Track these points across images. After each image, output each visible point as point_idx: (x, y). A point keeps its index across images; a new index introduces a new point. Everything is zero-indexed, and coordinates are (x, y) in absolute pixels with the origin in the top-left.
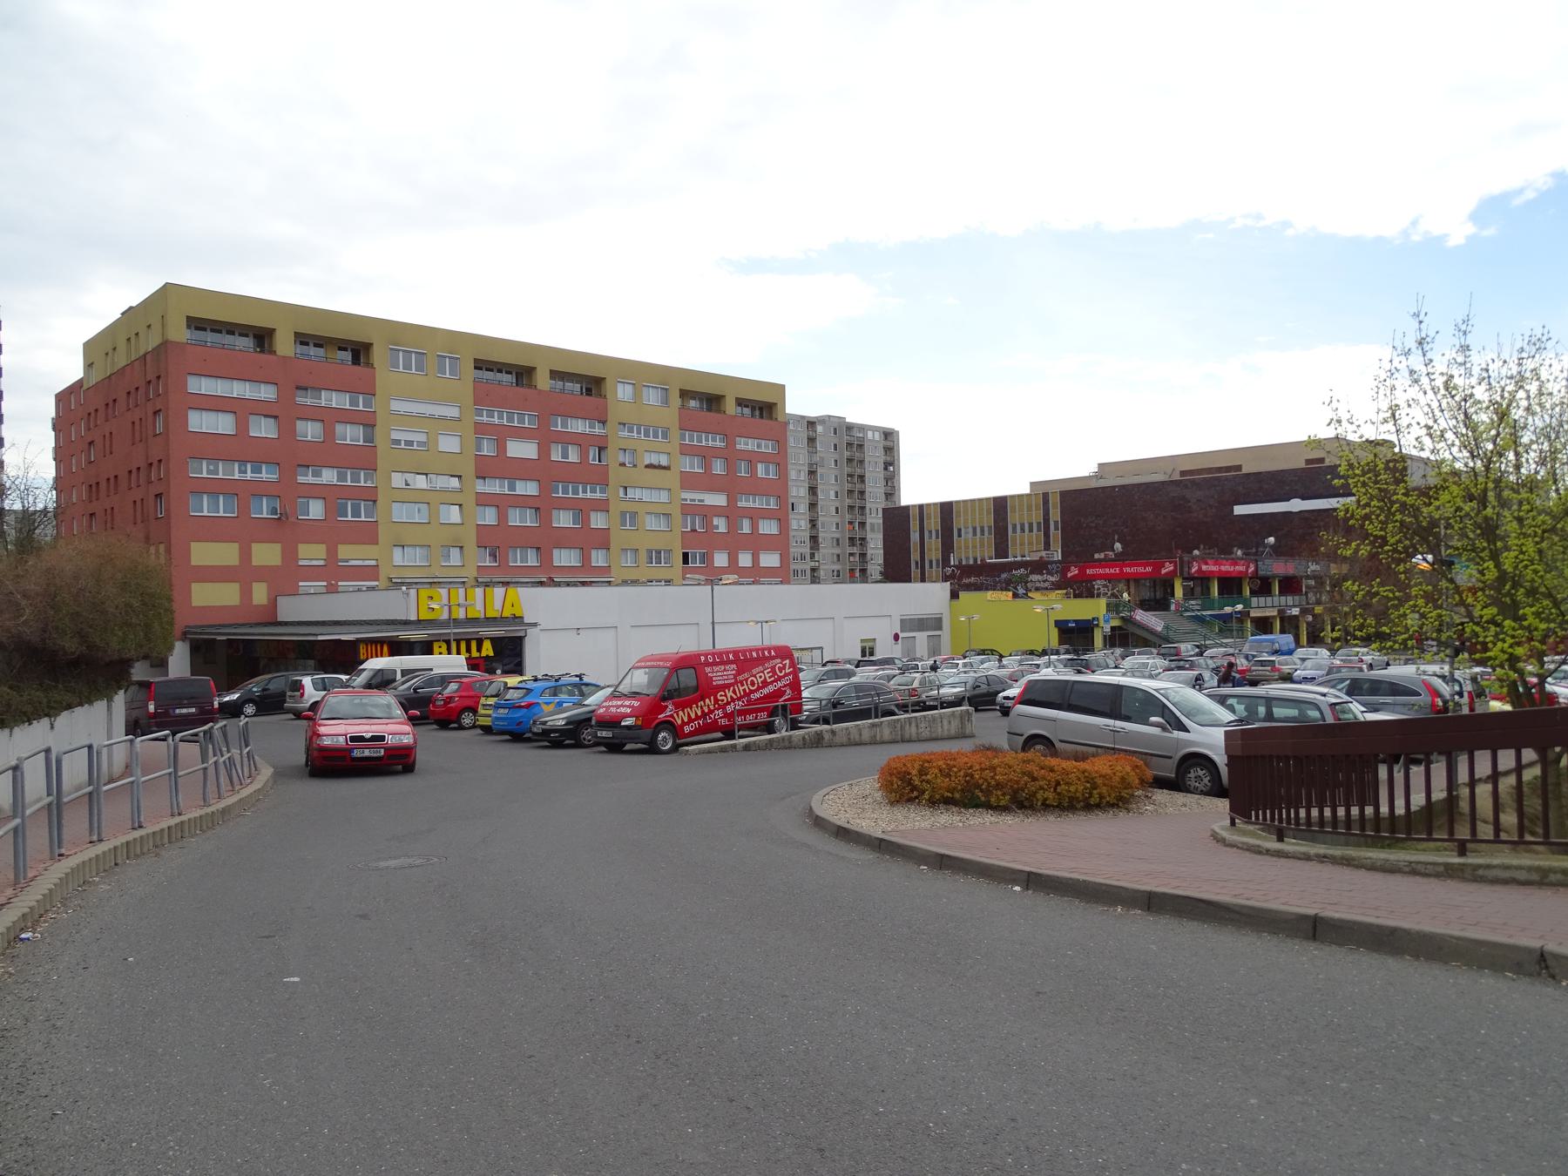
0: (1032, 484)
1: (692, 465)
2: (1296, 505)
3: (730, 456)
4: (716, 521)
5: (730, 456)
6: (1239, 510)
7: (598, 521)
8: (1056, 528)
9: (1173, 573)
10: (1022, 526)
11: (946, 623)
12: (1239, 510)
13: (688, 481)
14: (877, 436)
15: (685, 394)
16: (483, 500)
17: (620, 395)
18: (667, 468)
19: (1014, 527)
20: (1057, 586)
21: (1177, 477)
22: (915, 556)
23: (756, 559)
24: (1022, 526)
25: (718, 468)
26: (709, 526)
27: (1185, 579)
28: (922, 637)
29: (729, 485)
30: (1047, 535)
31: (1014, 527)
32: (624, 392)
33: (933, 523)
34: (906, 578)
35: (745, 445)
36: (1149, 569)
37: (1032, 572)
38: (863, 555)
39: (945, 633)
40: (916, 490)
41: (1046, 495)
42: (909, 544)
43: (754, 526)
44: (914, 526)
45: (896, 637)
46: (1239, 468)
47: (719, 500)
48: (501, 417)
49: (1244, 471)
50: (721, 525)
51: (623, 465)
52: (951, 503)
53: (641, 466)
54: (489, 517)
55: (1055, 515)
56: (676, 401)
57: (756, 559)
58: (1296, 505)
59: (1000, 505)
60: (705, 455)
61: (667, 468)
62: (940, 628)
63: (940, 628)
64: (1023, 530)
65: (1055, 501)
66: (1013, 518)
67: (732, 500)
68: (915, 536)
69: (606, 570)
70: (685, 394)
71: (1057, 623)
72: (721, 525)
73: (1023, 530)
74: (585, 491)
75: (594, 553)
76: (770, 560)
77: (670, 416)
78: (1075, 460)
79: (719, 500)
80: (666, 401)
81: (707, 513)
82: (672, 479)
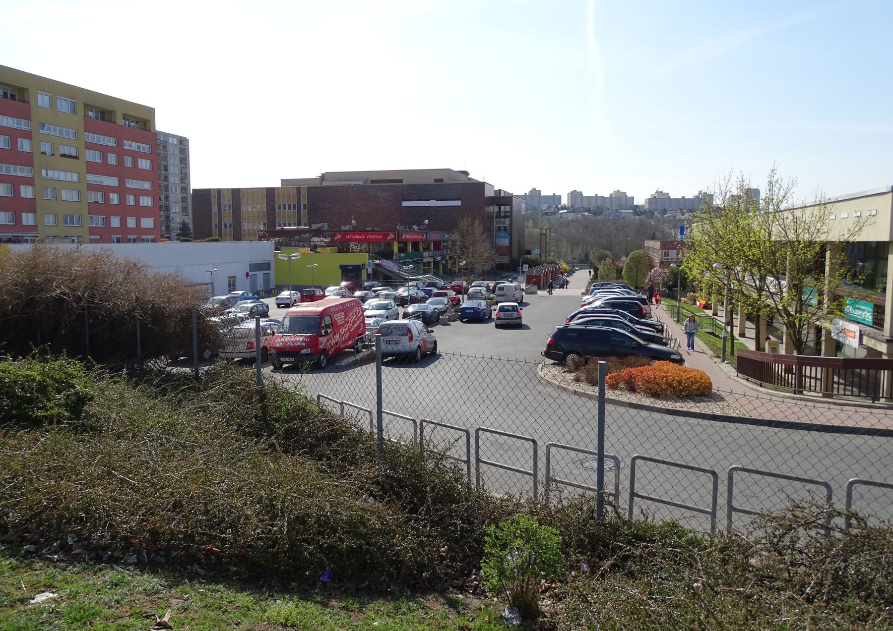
0: (282, 180)
1: (94, 156)
2: (433, 203)
3: (121, 153)
4: (111, 195)
5: (121, 153)
6: (405, 204)
7: (26, 192)
8: (305, 208)
9: (394, 239)
10: (284, 206)
11: (273, 266)
12: (405, 204)
13: (92, 168)
14: (175, 141)
15: (87, 106)
16: (92, 187)
17: (40, 103)
18: (76, 158)
19: (279, 206)
20: (328, 245)
21: (369, 184)
22: (215, 221)
23: (138, 222)
24: (284, 206)
25: (112, 159)
26: (106, 198)
27: (399, 243)
28: (260, 274)
29: (119, 172)
30: (299, 212)
31: (279, 206)
32: (43, 100)
33: (227, 201)
34: (240, 239)
35: (131, 146)
36: (381, 237)
37: (314, 236)
38: (167, 217)
39: (272, 272)
40: (201, 178)
41: (298, 189)
42: (213, 216)
43: (137, 201)
44: (214, 202)
45: (247, 275)
46: (401, 181)
47: (113, 182)
48: (55, 131)
49: (404, 183)
50: (114, 198)
51: (44, 153)
52: (239, 189)
53: (57, 155)
54: (98, 197)
55: (304, 201)
56: (80, 110)
57: (138, 222)
58: (433, 203)
59: (270, 193)
60: (104, 150)
61: (76, 158)
62: (269, 269)
63: (269, 269)
64: (284, 208)
65: (304, 193)
66: (279, 201)
67: (122, 182)
68: (215, 209)
69: (33, 228)
70: (87, 106)
71: (341, 267)
72: (114, 198)
73: (284, 208)
74: (15, 171)
75: (24, 215)
76: (147, 223)
77: (78, 120)
78: (309, 170)
79: (113, 182)
80: (74, 111)
81: (106, 190)
82: (80, 165)
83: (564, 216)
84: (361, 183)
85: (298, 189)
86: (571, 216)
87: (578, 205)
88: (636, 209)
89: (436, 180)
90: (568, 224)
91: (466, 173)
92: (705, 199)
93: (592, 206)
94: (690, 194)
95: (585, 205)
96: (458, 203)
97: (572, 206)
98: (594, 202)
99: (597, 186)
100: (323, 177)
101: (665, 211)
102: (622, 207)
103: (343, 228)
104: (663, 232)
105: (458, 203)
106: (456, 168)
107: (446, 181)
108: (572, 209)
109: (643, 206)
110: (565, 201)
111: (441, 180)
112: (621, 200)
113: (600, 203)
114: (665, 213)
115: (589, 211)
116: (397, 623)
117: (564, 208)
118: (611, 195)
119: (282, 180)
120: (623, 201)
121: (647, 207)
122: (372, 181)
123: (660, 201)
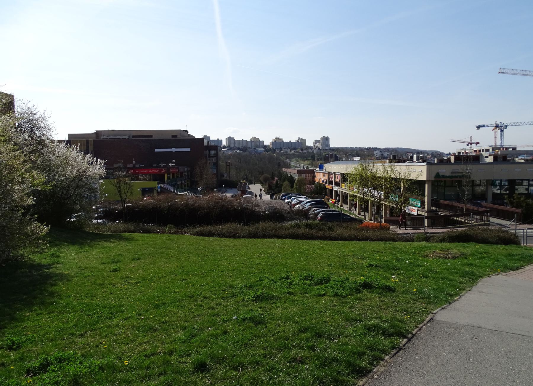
0: (69, 135)
2: (174, 150)
9: (165, 172)
46: (151, 136)
58: (174, 150)
83: (226, 152)
84: (127, 137)
85: (87, 141)
86: (230, 152)
87: (232, 145)
88: (265, 147)
89: (173, 136)
90: (229, 157)
91: (187, 131)
92: (301, 143)
93: (241, 146)
94: (294, 140)
95: (236, 145)
96: (189, 150)
97: (229, 146)
98: (241, 143)
99: (243, 135)
100: (98, 133)
101: (281, 149)
102: (257, 146)
103: (128, 166)
104: (283, 161)
105: (189, 150)
106: (183, 129)
107: (179, 137)
108: (229, 147)
109: (269, 146)
110: (224, 143)
111: (176, 136)
112: (256, 143)
113: (245, 144)
114: (281, 150)
115: (239, 149)
116: (248, 353)
117: (224, 147)
118: (251, 140)
119: (69, 135)
120: (258, 143)
121: (271, 146)
122: (133, 137)
123: (278, 143)
